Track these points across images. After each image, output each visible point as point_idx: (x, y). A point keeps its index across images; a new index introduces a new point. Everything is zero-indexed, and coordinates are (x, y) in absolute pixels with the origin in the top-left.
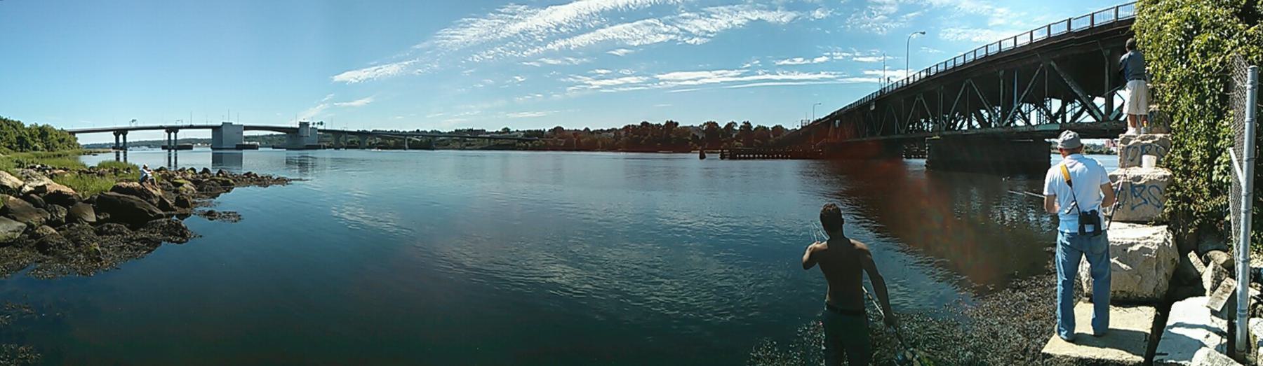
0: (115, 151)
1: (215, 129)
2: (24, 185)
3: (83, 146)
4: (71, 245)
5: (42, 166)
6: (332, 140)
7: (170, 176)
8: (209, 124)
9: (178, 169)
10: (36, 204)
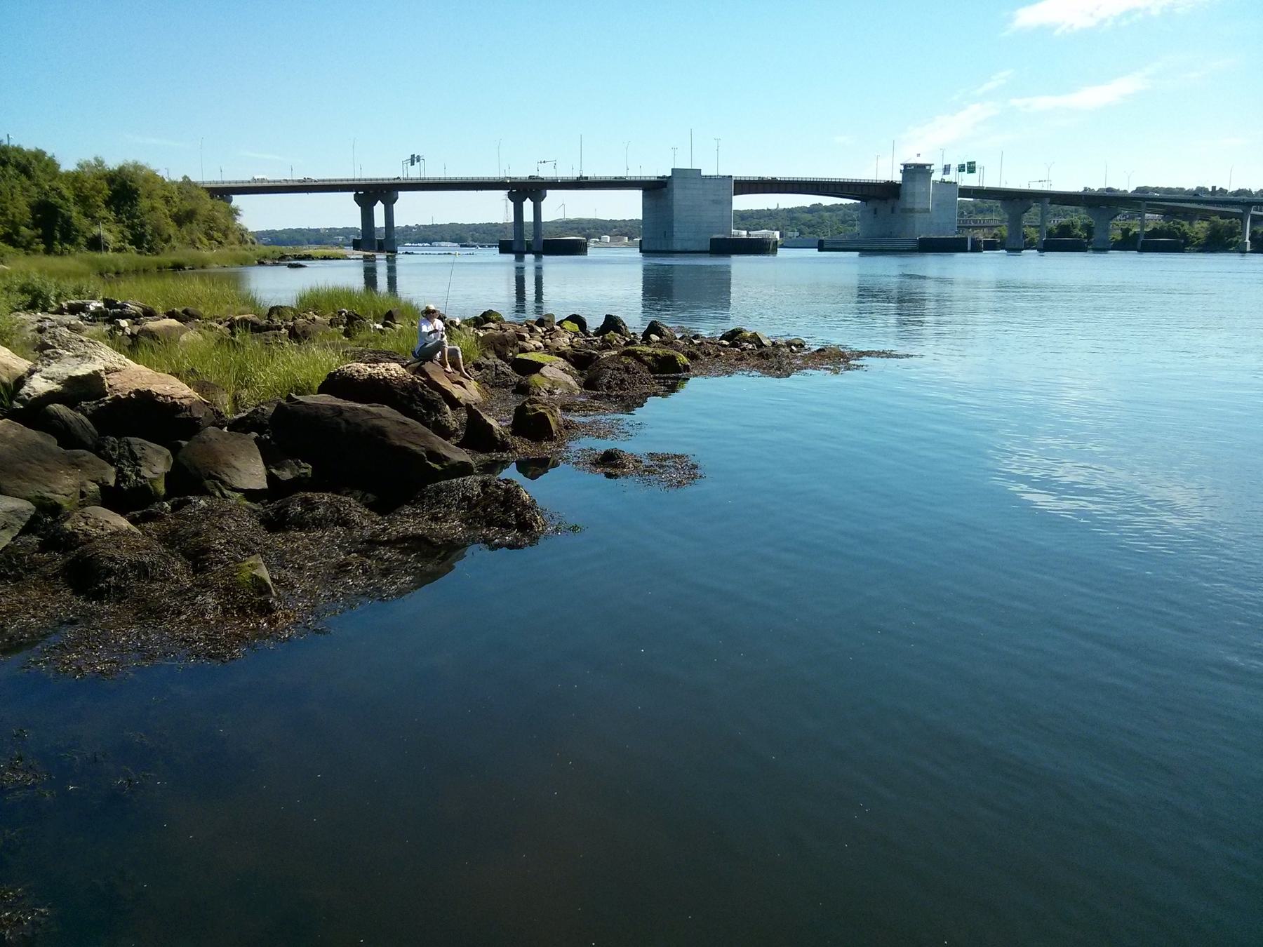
0: (360, 254)
1: (655, 189)
3: (260, 235)
4: (178, 566)
5: (109, 303)
8: (634, 173)
10: (66, 436)
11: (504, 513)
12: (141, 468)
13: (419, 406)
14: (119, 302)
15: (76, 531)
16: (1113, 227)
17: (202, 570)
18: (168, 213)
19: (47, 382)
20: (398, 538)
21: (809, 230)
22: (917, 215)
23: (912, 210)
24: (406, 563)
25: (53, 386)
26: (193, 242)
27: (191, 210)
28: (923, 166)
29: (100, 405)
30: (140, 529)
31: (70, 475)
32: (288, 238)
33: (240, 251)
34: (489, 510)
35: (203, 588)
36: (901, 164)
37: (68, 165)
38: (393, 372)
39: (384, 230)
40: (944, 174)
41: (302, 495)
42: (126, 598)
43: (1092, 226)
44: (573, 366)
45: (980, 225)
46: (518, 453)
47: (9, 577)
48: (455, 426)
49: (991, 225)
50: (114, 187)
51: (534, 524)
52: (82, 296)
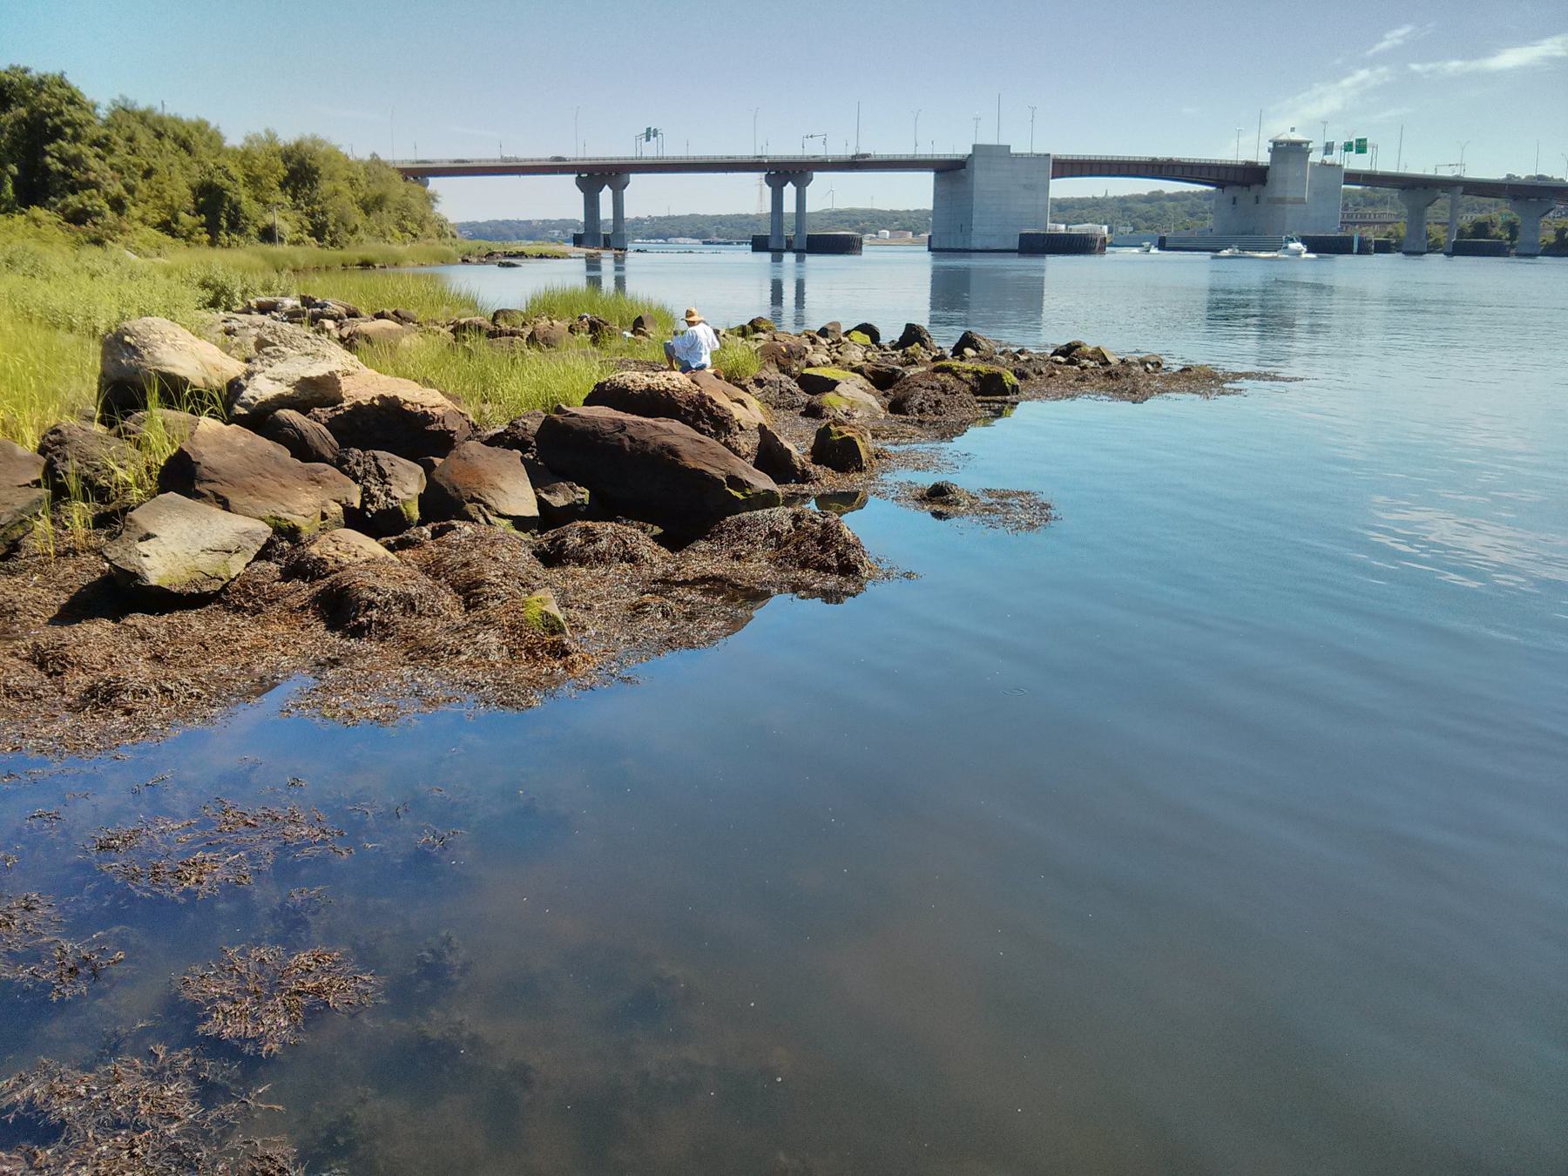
0: (583, 251)
1: (949, 171)
2: (249, 375)
3: (462, 227)
4: (448, 600)
5: (307, 301)
6: (1393, 213)
7: (790, 354)
8: (925, 150)
9: (816, 326)
10: (302, 449)
11: (823, 551)
12: (392, 487)
13: (707, 424)
14: (318, 301)
15: (325, 556)
16: (1544, 225)
17: (475, 606)
18: (354, 199)
19: (274, 384)
20: (695, 579)
21: (1146, 225)
22: (1289, 206)
23: (1282, 201)
24: (712, 607)
25: (285, 389)
26: (384, 235)
27: (381, 195)
28: (1298, 144)
29: (338, 413)
30: (398, 557)
31: (307, 492)
32: (493, 231)
33: (440, 246)
34: (803, 548)
35: (485, 625)
36: (1270, 141)
37: (234, 139)
38: (676, 383)
39: (612, 222)
40: (1326, 154)
41: (580, 523)
42: (391, 635)
43: (1517, 224)
44: (873, 385)
45: (1370, 220)
46: (822, 485)
47: (246, 610)
48: (746, 450)
49: (1382, 221)
50: (290, 165)
51: (859, 566)
52: (272, 293)
